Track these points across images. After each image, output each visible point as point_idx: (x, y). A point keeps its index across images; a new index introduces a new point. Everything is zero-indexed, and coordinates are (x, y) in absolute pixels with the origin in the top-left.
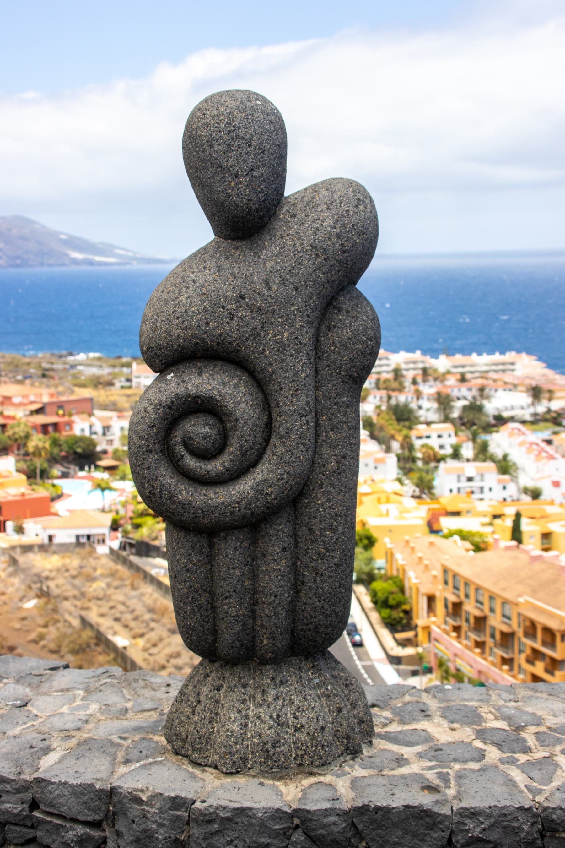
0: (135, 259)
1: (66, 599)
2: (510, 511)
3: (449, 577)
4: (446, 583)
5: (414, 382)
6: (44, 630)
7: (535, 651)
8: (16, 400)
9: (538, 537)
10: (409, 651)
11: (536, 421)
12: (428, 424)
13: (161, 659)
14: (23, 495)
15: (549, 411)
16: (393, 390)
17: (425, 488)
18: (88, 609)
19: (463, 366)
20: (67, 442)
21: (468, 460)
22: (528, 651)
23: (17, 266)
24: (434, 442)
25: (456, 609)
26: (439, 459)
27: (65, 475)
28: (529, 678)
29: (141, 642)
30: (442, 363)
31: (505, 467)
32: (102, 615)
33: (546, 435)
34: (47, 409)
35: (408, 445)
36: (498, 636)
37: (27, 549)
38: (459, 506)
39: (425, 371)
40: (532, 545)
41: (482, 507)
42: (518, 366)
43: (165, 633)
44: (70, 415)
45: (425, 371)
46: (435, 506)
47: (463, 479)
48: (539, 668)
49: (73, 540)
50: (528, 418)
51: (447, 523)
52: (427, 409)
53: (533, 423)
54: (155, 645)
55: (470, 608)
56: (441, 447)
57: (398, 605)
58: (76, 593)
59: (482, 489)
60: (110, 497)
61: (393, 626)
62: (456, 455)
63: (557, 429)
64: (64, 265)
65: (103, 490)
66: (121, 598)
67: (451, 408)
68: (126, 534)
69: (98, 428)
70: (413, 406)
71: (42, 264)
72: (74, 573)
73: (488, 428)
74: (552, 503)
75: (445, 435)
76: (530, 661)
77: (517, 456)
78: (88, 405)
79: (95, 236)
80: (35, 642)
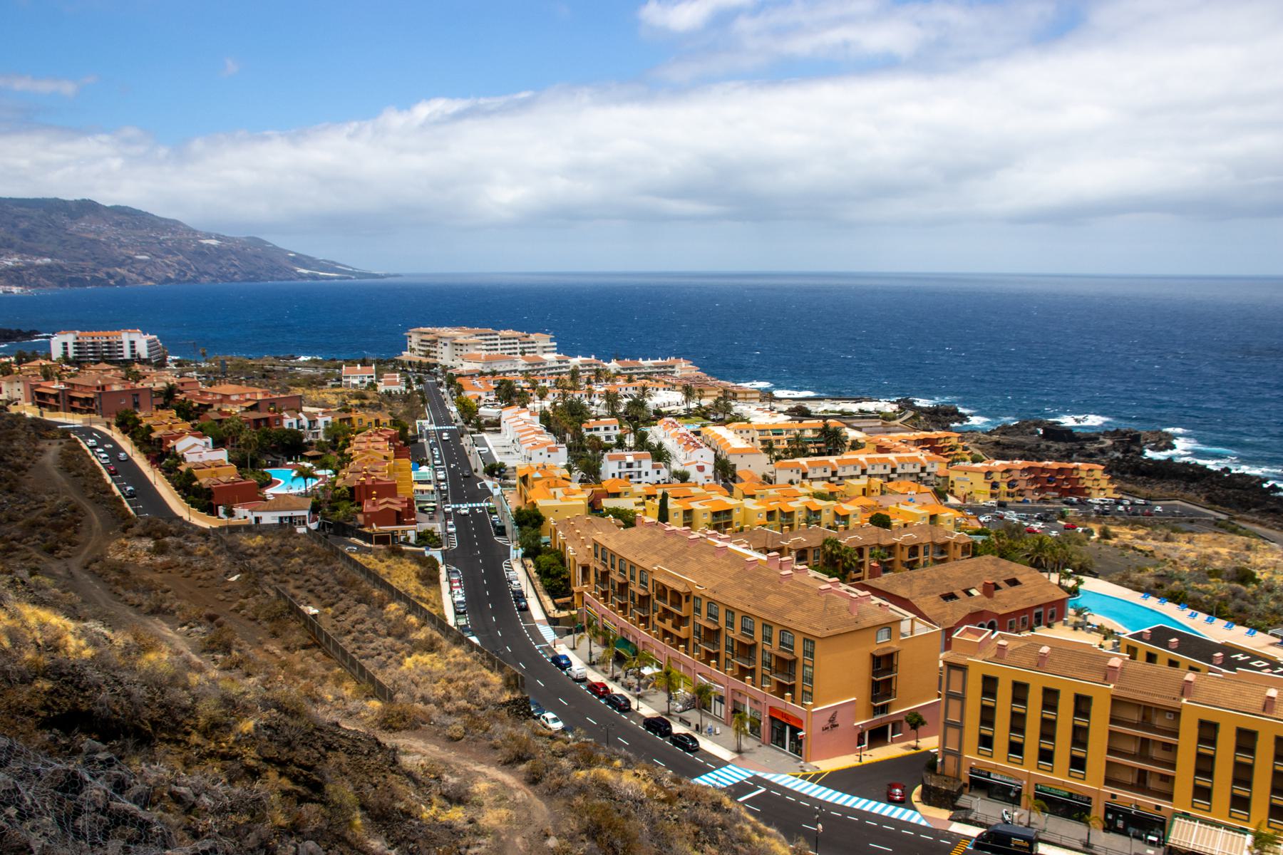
0: (353, 273)
1: (267, 573)
2: (659, 492)
3: (600, 551)
4: (596, 555)
5: (589, 382)
6: (245, 601)
7: (665, 610)
8: (234, 398)
9: (681, 514)
10: (564, 613)
11: (688, 415)
12: (597, 418)
13: (347, 625)
14: (233, 482)
15: (700, 406)
16: (570, 389)
17: (591, 473)
18: (286, 582)
19: (631, 369)
20: (276, 435)
21: (631, 449)
22: (660, 611)
23: (251, 280)
24: (602, 434)
25: (604, 577)
26: (607, 448)
27: (275, 465)
28: (661, 632)
29: (330, 611)
30: (613, 366)
31: (660, 455)
32: (298, 588)
33: (696, 427)
34: (260, 407)
35: (578, 436)
36: (637, 599)
37: (234, 529)
38: (620, 489)
39: (598, 372)
40: (675, 524)
41: (638, 489)
42: (677, 369)
43: (352, 602)
44: (281, 411)
45: (598, 372)
46: (598, 489)
47: (624, 465)
48: (668, 625)
49: (277, 521)
50: (682, 412)
51: (607, 503)
52: (598, 406)
53: (686, 417)
54: (343, 613)
55: (615, 576)
56: (608, 438)
57: (559, 574)
58: (275, 567)
59: (639, 473)
60: (312, 483)
61: (553, 593)
62: (620, 444)
63: (705, 422)
64: (291, 279)
65: (305, 478)
66: (315, 572)
67: (618, 404)
68: (324, 516)
69: (305, 422)
70: (586, 402)
71: (272, 279)
72: (275, 550)
73: (649, 422)
74: (696, 485)
75: (612, 428)
76: (661, 619)
77: (670, 444)
78: (298, 402)
79: (321, 254)
80: (236, 611)
